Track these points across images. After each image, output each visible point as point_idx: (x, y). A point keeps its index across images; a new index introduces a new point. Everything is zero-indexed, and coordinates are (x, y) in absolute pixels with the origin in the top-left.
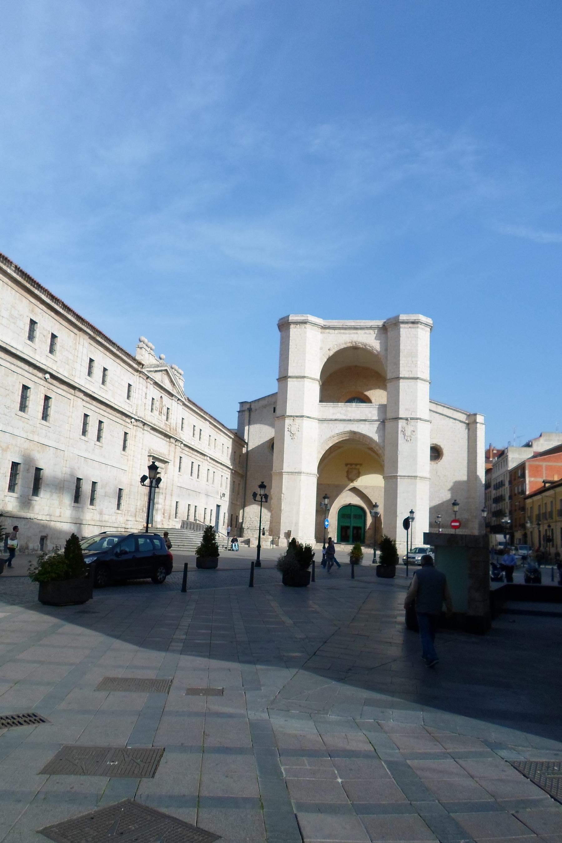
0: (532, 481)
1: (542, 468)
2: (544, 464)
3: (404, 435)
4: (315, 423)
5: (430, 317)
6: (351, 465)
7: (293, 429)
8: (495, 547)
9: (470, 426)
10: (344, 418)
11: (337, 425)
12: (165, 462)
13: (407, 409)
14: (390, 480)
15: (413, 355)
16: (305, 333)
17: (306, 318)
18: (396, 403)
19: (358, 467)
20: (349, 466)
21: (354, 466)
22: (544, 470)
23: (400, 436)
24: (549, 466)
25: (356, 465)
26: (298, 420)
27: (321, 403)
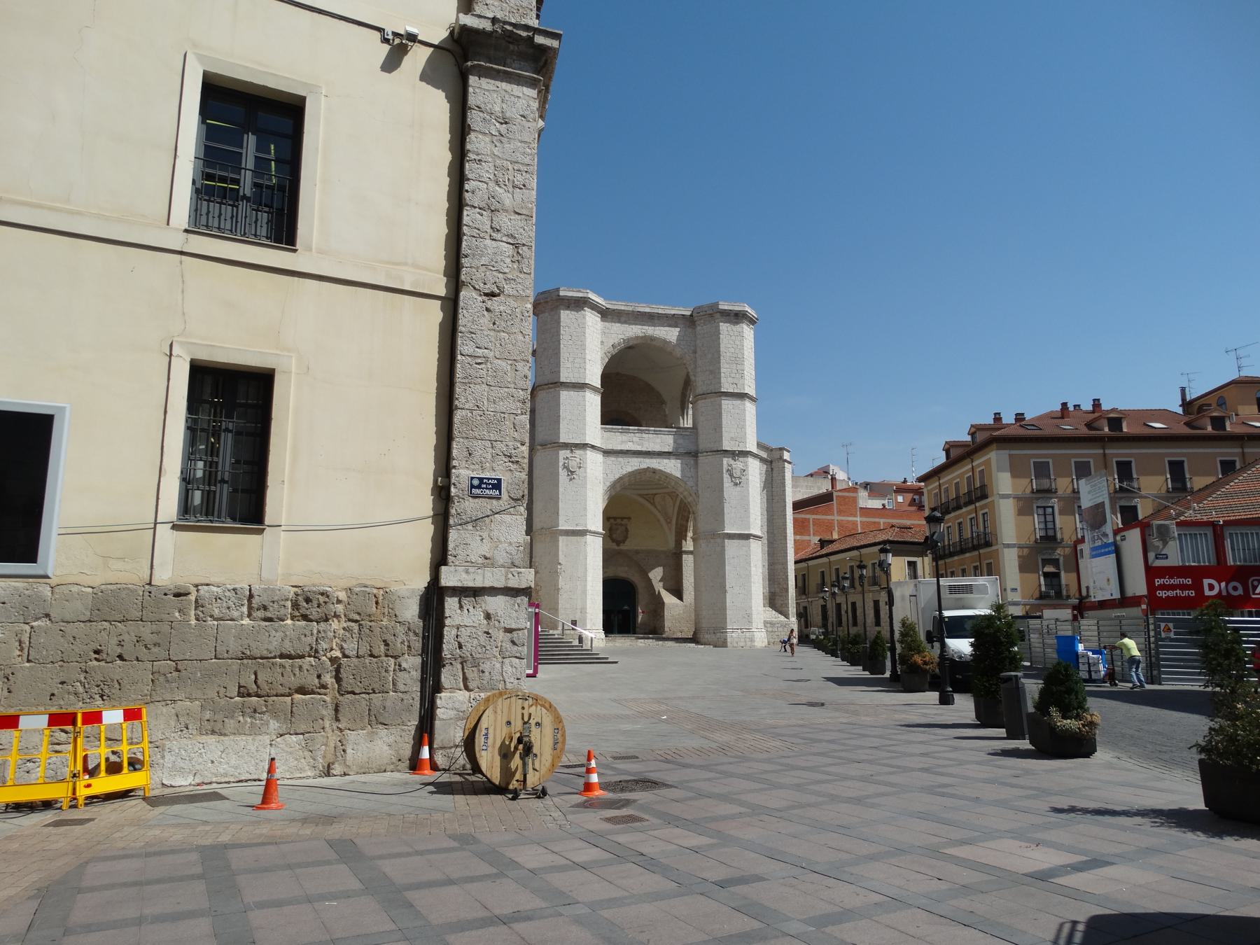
0: (798, 540)
1: (809, 522)
2: (811, 517)
3: (731, 475)
4: (599, 457)
5: (444, 313)
6: (615, 518)
7: (573, 465)
8: (1234, 653)
9: (774, 464)
10: (639, 448)
11: (630, 459)
12: (629, 518)
13: (732, 439)
14: (712, 541)
15: (738, 360)
16: (584, 318)
17: (585, 295)
18: (716, 429)
19: (625, 521)
20: (612, 521)
21: (619, 521)
22: (811, 526)
23: (726, 476)
24: (817, 519)
25: (622, 519)
26: (578, 452)
27: (605, 426)
